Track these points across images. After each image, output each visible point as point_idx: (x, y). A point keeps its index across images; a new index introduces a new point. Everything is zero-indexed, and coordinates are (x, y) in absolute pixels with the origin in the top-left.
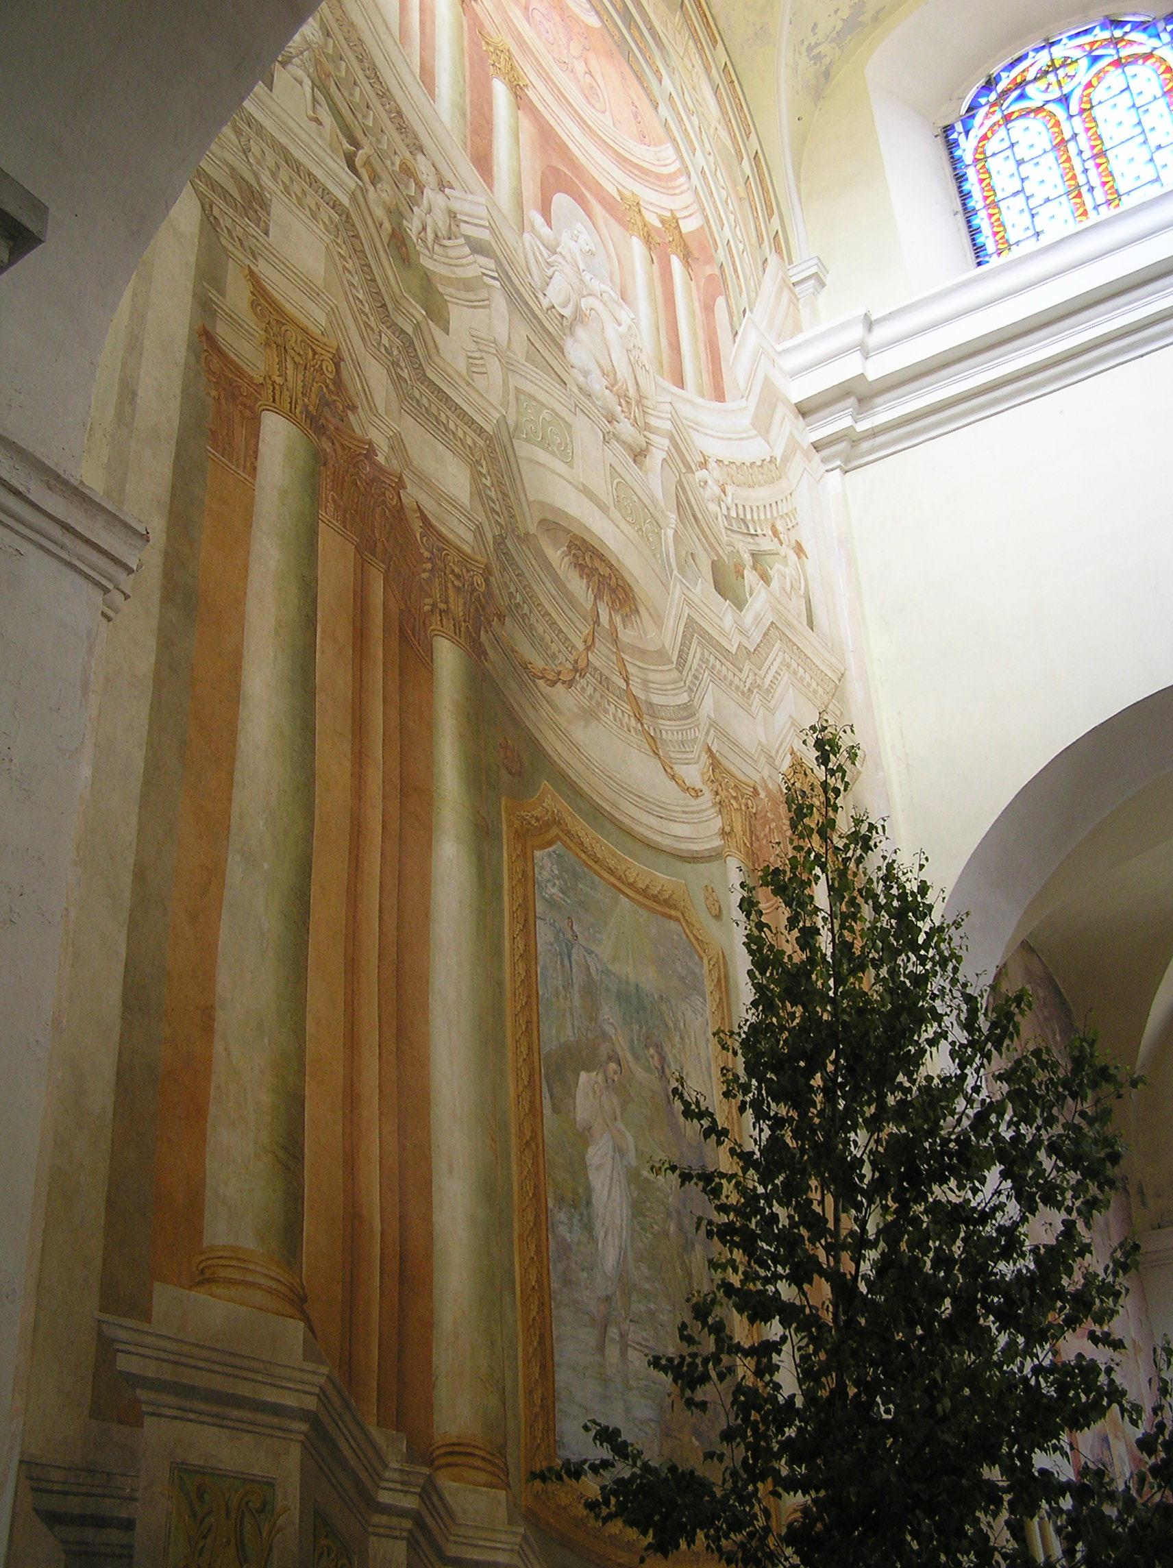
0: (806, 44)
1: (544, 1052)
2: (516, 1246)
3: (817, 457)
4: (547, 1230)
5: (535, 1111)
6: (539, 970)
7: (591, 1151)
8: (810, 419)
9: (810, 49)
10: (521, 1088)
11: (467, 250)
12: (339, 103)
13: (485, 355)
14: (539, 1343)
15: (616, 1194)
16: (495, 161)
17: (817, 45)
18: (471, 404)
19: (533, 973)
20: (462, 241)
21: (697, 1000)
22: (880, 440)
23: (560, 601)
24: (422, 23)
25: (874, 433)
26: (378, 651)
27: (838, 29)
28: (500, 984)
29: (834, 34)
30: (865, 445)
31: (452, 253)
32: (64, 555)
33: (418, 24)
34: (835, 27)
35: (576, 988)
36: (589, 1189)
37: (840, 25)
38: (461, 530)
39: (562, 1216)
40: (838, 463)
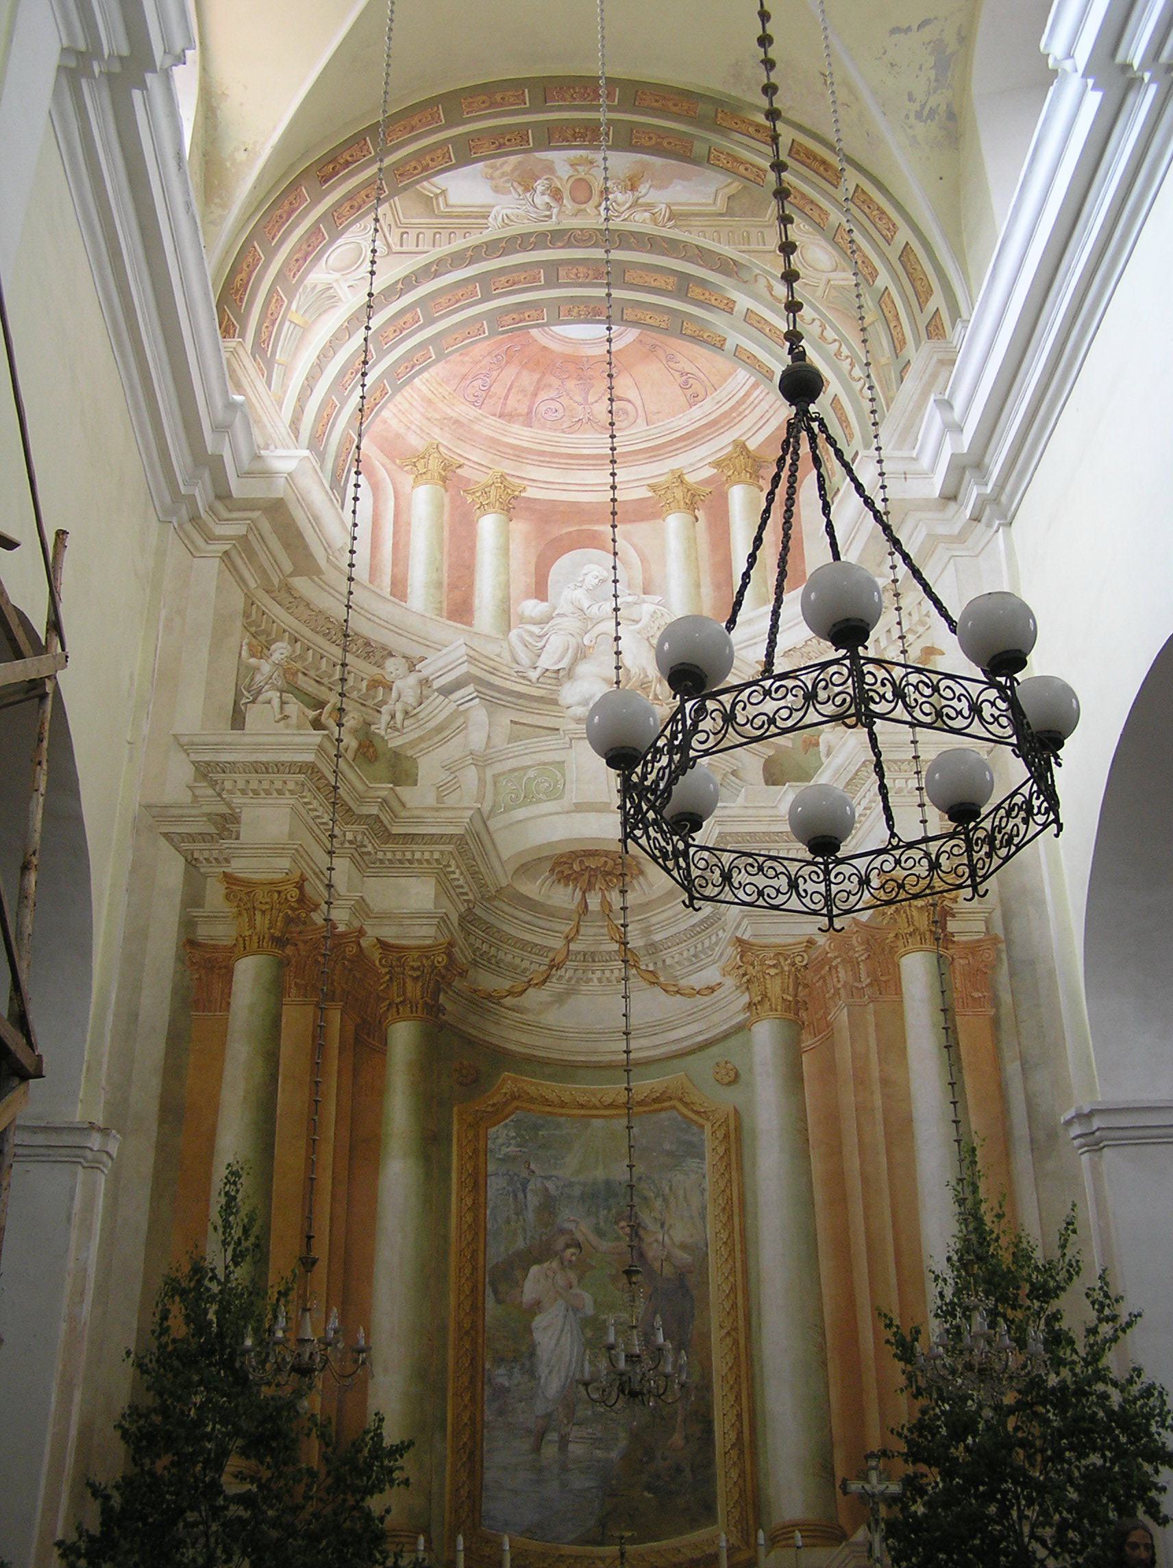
0: (912, 116)
1: (489, 1267)
2: (450, 1402)
3: (981, 527)
4: (483, 1383)
5: (476, 1308)
6: (488, 1212)
7: (538, 1319)
8: (960, 497)
9: (918, 115)
10: (462, 1298)
11: (442, 698)
12: (304, 686)
13: (457, 773)
14: (469, 1458)
15: (566, 1340)
16: (477, 593)
17: (923, 107)
18: (439, 824)
19: (481, 1216)
20: (436, 694)
21: (692, 1163)
22: (1008, 489)
23: (536, 921)
24: (395, 545)
25: (1001, 486)
26: (334, 1065)
27: (933, 78)
28: (445, 1238)
29: (933, 84)
30: (1004, 499)
31: (421, 715)
32: (51, 1159)
33: (390, 549)
34: (929, 79)
35: (530, 1210)
36: (533, 1347)
37: (932, 74)
38: (424, 931)
39: (502, 1371)
40: (997, 522)
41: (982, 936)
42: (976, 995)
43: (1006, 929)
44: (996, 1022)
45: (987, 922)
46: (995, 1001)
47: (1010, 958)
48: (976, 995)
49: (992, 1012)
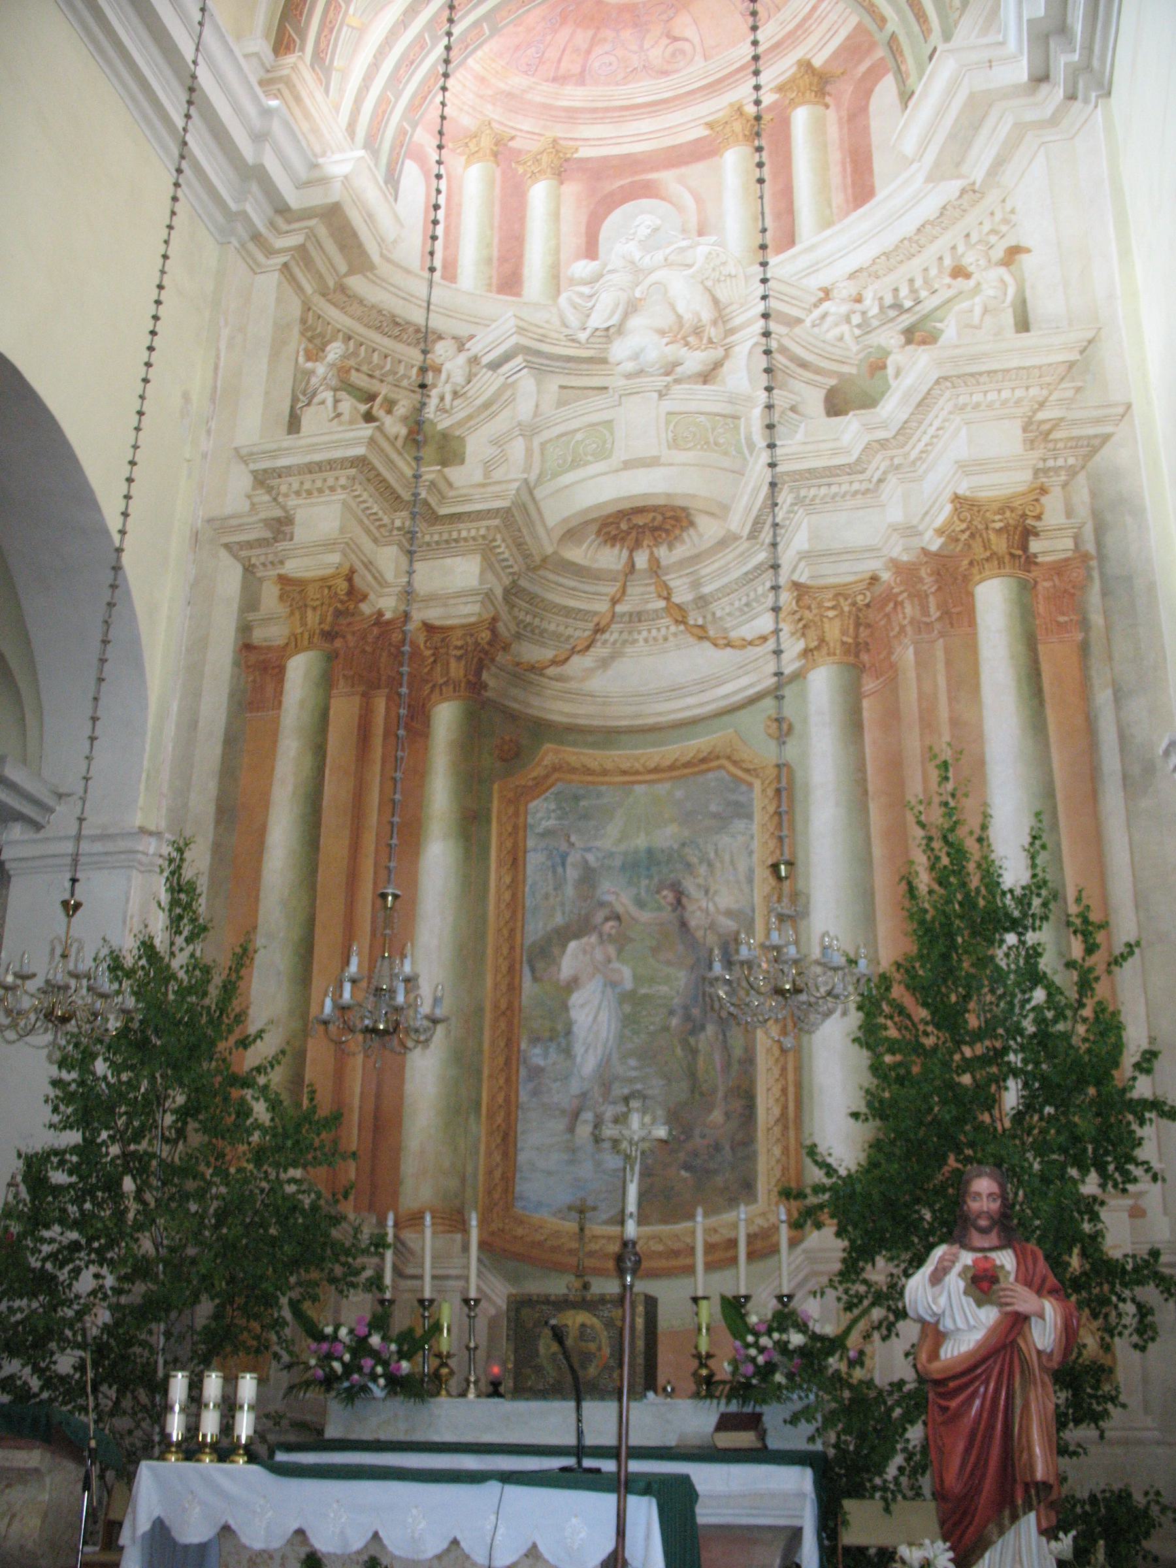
41: (1069, 554)
42: (1062, 619)
43: (1099, 544)
44: (1084, 649)
45: (1077, 538)
46: (1084, 624)
47: (1102, 575)
48: (1062, 619)
49: (1080, 636)
